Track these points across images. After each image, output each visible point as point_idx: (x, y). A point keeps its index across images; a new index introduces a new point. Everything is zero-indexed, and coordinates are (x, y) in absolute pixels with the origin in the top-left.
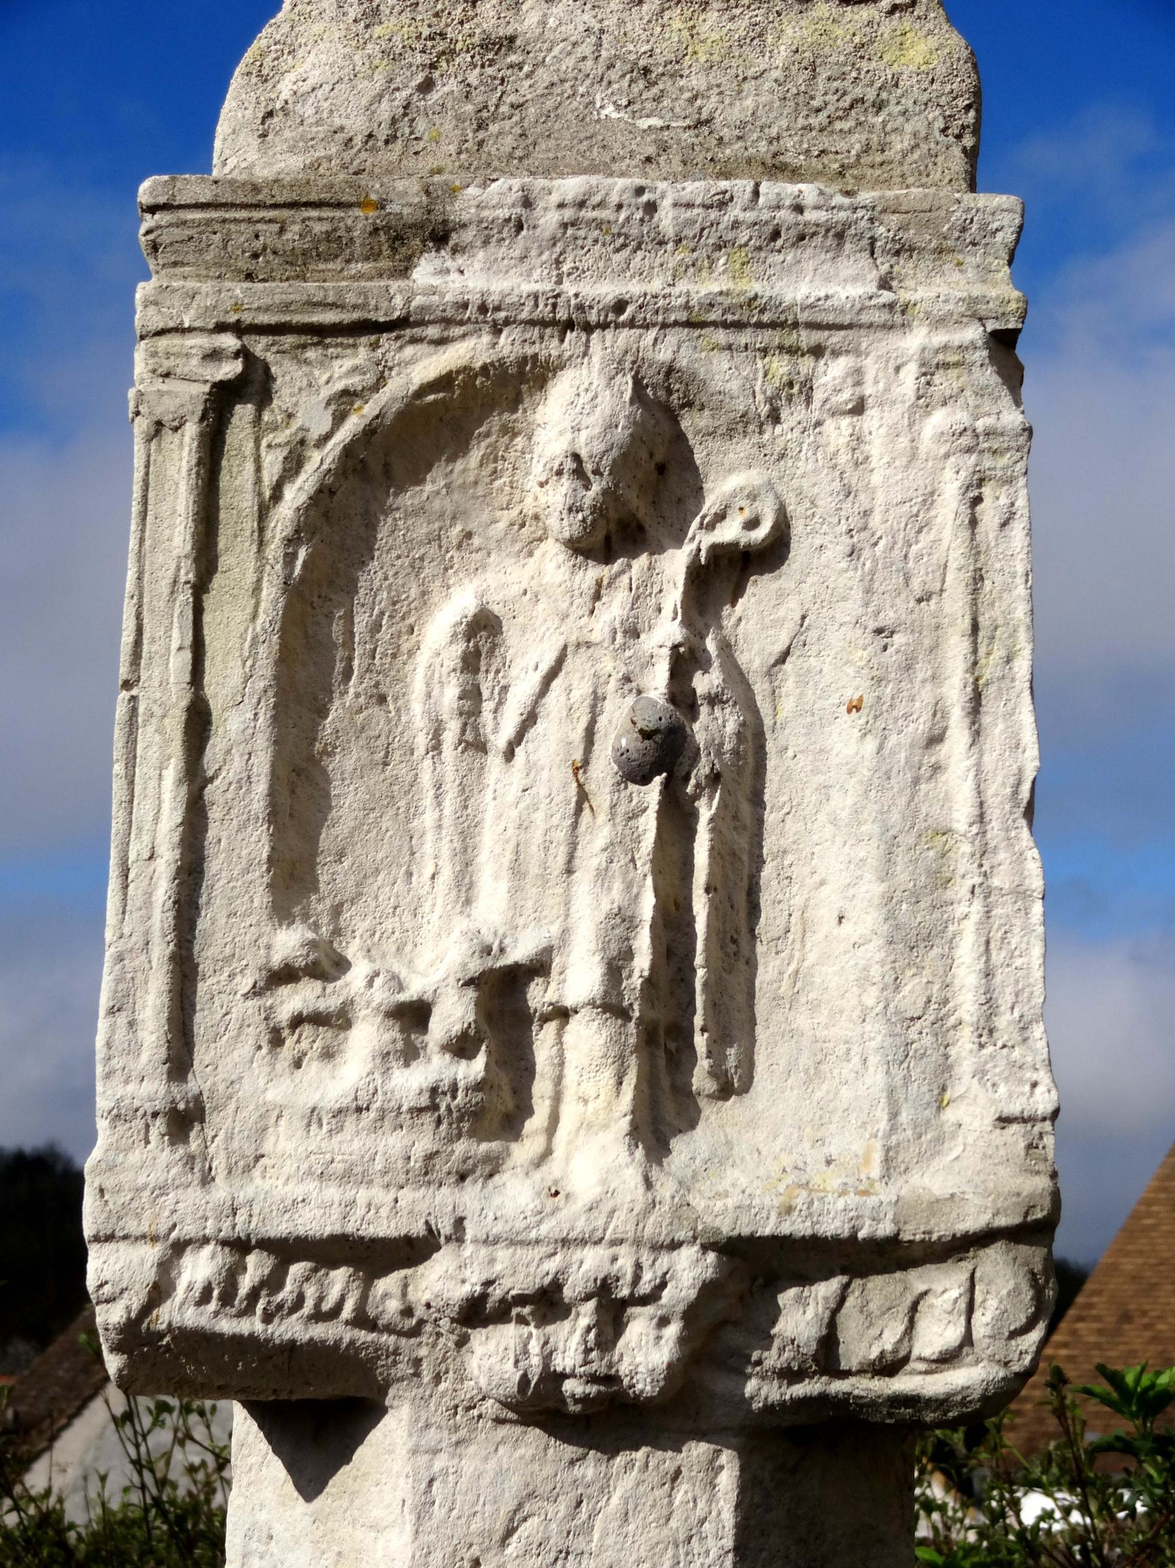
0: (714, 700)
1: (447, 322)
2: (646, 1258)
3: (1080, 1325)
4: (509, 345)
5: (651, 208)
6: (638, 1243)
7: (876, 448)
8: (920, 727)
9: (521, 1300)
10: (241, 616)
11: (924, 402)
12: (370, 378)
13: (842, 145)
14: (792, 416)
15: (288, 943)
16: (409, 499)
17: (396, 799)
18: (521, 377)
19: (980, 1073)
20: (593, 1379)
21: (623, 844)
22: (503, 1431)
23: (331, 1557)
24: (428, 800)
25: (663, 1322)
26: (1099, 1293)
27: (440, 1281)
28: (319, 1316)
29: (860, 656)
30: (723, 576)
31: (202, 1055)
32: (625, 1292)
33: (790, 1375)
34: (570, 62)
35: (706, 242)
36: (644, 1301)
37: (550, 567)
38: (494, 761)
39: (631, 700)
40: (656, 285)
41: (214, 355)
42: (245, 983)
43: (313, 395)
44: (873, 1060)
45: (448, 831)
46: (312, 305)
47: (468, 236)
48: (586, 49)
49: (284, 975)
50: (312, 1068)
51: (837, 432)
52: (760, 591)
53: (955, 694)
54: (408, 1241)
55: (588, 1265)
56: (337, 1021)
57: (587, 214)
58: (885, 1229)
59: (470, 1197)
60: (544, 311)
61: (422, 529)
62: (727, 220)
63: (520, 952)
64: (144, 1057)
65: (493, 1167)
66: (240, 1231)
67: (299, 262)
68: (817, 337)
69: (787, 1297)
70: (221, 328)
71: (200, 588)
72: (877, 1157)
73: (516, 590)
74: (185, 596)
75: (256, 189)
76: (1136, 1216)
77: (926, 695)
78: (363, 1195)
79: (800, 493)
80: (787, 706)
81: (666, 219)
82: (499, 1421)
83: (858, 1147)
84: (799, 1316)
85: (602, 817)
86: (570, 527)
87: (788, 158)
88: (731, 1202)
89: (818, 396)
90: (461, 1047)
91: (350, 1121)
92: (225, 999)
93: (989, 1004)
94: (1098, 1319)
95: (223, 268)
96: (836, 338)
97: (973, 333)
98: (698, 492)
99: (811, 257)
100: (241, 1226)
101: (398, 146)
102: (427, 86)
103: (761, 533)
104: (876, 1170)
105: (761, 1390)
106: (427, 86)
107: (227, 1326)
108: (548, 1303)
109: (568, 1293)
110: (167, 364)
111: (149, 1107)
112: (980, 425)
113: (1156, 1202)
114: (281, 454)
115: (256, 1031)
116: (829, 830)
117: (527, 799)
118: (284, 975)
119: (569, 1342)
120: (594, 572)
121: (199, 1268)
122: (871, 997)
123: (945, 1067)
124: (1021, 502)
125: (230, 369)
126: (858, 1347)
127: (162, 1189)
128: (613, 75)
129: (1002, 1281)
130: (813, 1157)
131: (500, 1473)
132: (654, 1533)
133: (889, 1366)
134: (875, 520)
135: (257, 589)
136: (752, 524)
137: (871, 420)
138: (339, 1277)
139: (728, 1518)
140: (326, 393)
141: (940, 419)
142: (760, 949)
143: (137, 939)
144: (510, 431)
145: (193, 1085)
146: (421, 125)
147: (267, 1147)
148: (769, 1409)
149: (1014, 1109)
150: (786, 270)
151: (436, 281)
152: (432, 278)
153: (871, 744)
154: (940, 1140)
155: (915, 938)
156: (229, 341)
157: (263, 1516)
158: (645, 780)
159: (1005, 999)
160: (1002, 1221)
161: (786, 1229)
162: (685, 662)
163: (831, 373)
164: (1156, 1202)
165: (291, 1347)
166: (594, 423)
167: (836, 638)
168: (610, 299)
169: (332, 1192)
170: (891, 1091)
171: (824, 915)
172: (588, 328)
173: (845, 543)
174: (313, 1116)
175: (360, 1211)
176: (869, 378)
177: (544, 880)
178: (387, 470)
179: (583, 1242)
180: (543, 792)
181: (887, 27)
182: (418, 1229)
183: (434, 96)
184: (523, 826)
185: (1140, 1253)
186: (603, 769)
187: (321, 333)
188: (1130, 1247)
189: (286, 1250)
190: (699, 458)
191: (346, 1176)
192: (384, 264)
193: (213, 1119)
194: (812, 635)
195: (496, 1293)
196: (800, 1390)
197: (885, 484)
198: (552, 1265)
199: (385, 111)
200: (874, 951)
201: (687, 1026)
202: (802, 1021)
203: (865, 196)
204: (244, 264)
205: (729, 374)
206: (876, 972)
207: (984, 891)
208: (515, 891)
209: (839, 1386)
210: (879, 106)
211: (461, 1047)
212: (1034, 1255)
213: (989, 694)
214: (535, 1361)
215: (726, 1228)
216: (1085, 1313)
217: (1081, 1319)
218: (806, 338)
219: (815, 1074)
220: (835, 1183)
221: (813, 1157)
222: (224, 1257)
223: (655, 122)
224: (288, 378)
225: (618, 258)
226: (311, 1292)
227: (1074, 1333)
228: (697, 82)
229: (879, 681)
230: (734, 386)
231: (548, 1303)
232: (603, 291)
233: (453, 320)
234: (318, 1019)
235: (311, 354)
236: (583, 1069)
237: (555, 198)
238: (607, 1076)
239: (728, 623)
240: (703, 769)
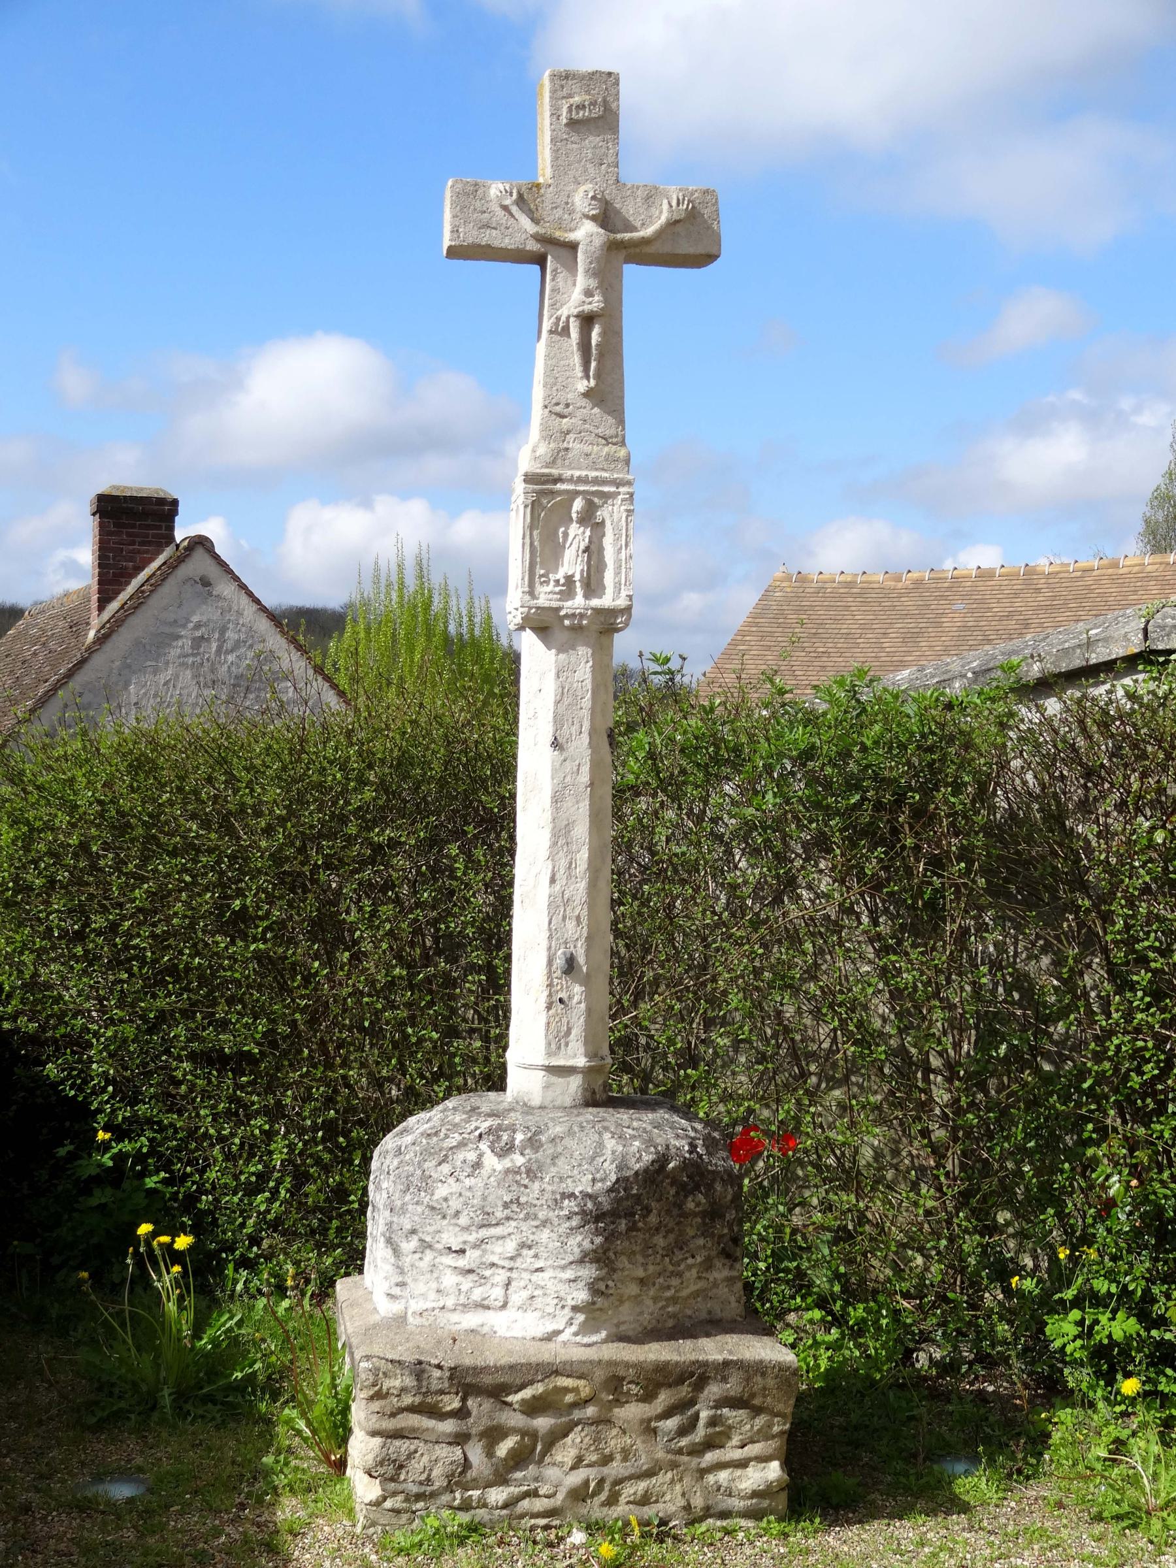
113: (750, 633)
164: (750, 633)
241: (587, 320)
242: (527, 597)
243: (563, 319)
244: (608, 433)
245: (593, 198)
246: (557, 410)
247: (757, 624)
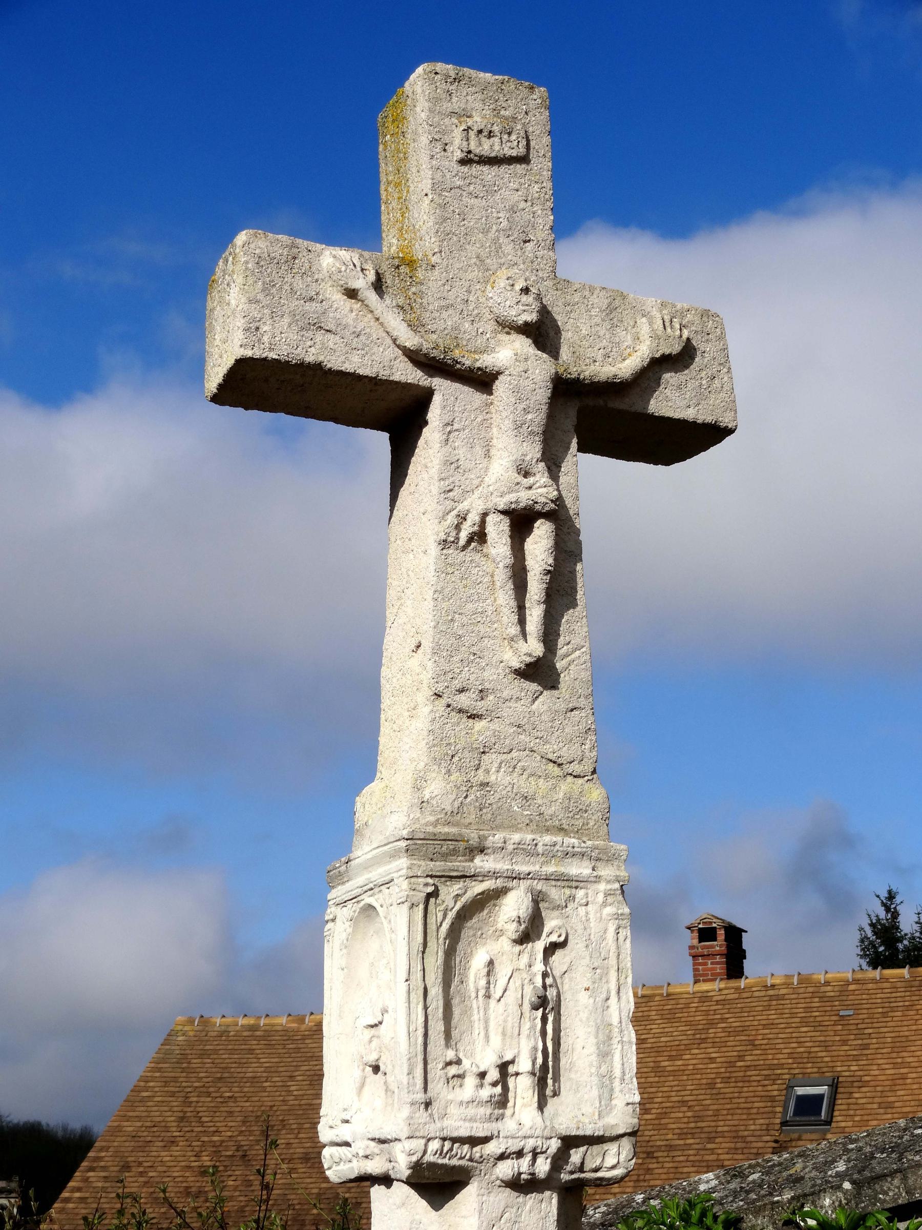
0: (551, 986)
1: (485, 876)
2: (544, 1141)
3: (91, 1174)
4: (499, 883)
5: (536, 845)
6: (542, 1137)
7: (591, 916)
8: (604, 996)
9: (514, 1153)
10: (433, 960)
11: (604, 904)
12: (463, 891)
13: (577, 823)
14: (571, 906)
15: (450, 1055)
16: (469, 924)
17: (467, 1011)
18: (501, 891)
19: (621, 1091)
20: (530, 1174)
21: (533, 1027)
22: (500, 1189)
23: (446, 1227)
24: (476, 1012)
25: (547, 1158)
26: (106, 1149)
27: (493, 1148)
28: (461, 1158)
29: (589, 975)
30: (551, 949)
31: (430, 1086)
32: (539, 1151)
33: (572, 1173)
34: (505, 792)
35: (550, 855)
36: (542, 1153)
37: (505, 945)
38: (492, 1002)
39: (532, 986)
40: (537, 868)
41: (426, 885)
42: (440, 1066)
43: (453, 896)
44: (594, 1087)
45: (482, 1022)
46: (451, 870)
47: (489, 851)
48: (509, 789)
49: (449, 1063)
50: (457, 1090)
51: (582, 910)
52: (559, 954)
53: (613, 986)
54: (486, 1137)
55: (530, 1144)
56: (461, 1076)
57: (521, 846)
58: (601, 1133)
59: (499, 1125)
60: (509, 874)
61: (471, 933)
62: (555, 850)
63: (508, 1058)
64: (418, 1087)
65: (502, 1117)
66: (445, 1135)
67: (445, 856)
68: (577, 884)
69: (572, 1151)
70: (427, 876)
71: (423, 952)
72: (597, 1114)
73: (497, 952)
74: (420, 955)
75: (435, 835)
76: (136, 1090)
77: (605, 988)
78: (475, 1125)
79: (572, 927)
80: (566, 987)
81: (540, 849)
82: (500, 1186)
83: (591, 1110)
84: (576, 1156)
85: (527, 1020)
86: (515, 936)
87: (563, 826)
88: (565, 1126)
89: (577, 900)
90: (494, 1084)
91: (470, 1104)
92: (436, 1069)
93: (624, 1073)
94: (104, 1168)
95: (425, 857)
96: (582, 884)
97: (617, 886)
98: (543, 925)
99: (575, 861)
100: (445, 1134)
101: (459, 815)
102: (466, 797)
103: (562, 939)
104: (596, 1117)
105: (565, 1177)
106: (466, 797)
107: (440, 1161)
108: (520, 1154)
109: (525, 1151)
110: (414, 887)
111: (421, 1101)
112: (620, 912)
113: (153, 1079)
114: (442, 913)
115: (443, 1080)
116: (579, 1023)
117: (506, 1014)
118: (449, 1063)
119: (524, 1164)
120: (518, 948)
121: (434, 1145)
122: (593, 1070)
123: (612, 1090)
124: (629, 934)
125: (430, 889)
126: (589, 1165)
127: (425, 1124)
128: (517, 797)
129: (626, 1145)
130: (579, 1114)
131: (500, 1200)
132: (537, 1216)
133: (596, 1170)
134: (592, 936)
135: (437, 952)
136: (560, 936)
137: (590, 907)
138: (466, 1147)
139: (555, 1212)
140: (453, 895)
141: (609, 910)
142: (561, 1055)
143: (414, 1054)
144: (495, 905)
145: (429, 1094)
146: (465, 809)
147: (448, 1111)
148: (566, 1182)
149: (630, 1101)
150: (569, 864)
151: (481, 864)
152: (481, 863)
153: (592, 1000)
154: (611, 1109)
155: (604, 1055)
156: (430, 880)
157: (417, 1217)
158: (537, 1009)
159: (627, 1071)
160: (628, 1131)
161: (578, 1133)
162: (545, 975)
163: (580, 893)
164: (153, 1079)
165: (454, 1167)
166: (524, 907)
167: (581, 969)
168: (527, 872)
169: (467, 1124)
170: (600, 1096)
171: (578, 1047)
172: (520, 879)
173: (584, 944)
174: (461, 1103)
175: (474, 1129)
176: (590, 895)
177: (512, 1037)
178: (465, 916)
179: (529, 1137)
180: (511, 1012)
181: (587, 786)
182: (489, 1134)
183: (468, 799)
184: (505, 1021)
185: (139, 1118)
186: (527, 1007)
187: (451, 878)
188: (131, 1114)
189: (454, 1140)
190: (543, 914)
191: (471, 1120)
192: (467, 858)
193: (433, 1104)
194: (574, 967)
195: (508, 1151)
196: (574, 1176)
197: (595, 927)
198: (522, 1143)
199: (456, 804)
200: (594, 1058)
201: (546, 1079)
202: (573, 1076)
203: (589, 843)
204: (431, 856)
205: (556, 894)
206: (595, 1063)
207: (621, 1042)
208: (504, 1039)
209: (582, 1175)
210: (586, 811)
211: (494, 1084)
212: (633, 1139)
213: (621, 988)
214: (516, 1169)
215: (564, 1134)
216: (95, 1165)
217: (92, 1169)
218: (574, 884)
219: (577, 1091)
220: (587, 1121)
221: (579, 1114)
222: (441, 1142)
223: (528, 812)
224: (443, 890)
225: (527, 859)
226: (459, 1151)
227: (86, 1180)
228: (540, 802)
229: (594, 982)
230: (556, 897)
231: (520, 1154)
232: (524, 869)
233: (486, 876)
234: (459, 1076)
235: (448, 883)
236: (523, 1088)
237: (512, 841)
238: (531, 1091)
239: (551, 962)
240: (550, 1006)
241: (521, 521)
242: (422, 1115)
243: (473, 518)
244: (566, 753)
245: (526, 291)
246: (461, 705)
247: (160, 1070)
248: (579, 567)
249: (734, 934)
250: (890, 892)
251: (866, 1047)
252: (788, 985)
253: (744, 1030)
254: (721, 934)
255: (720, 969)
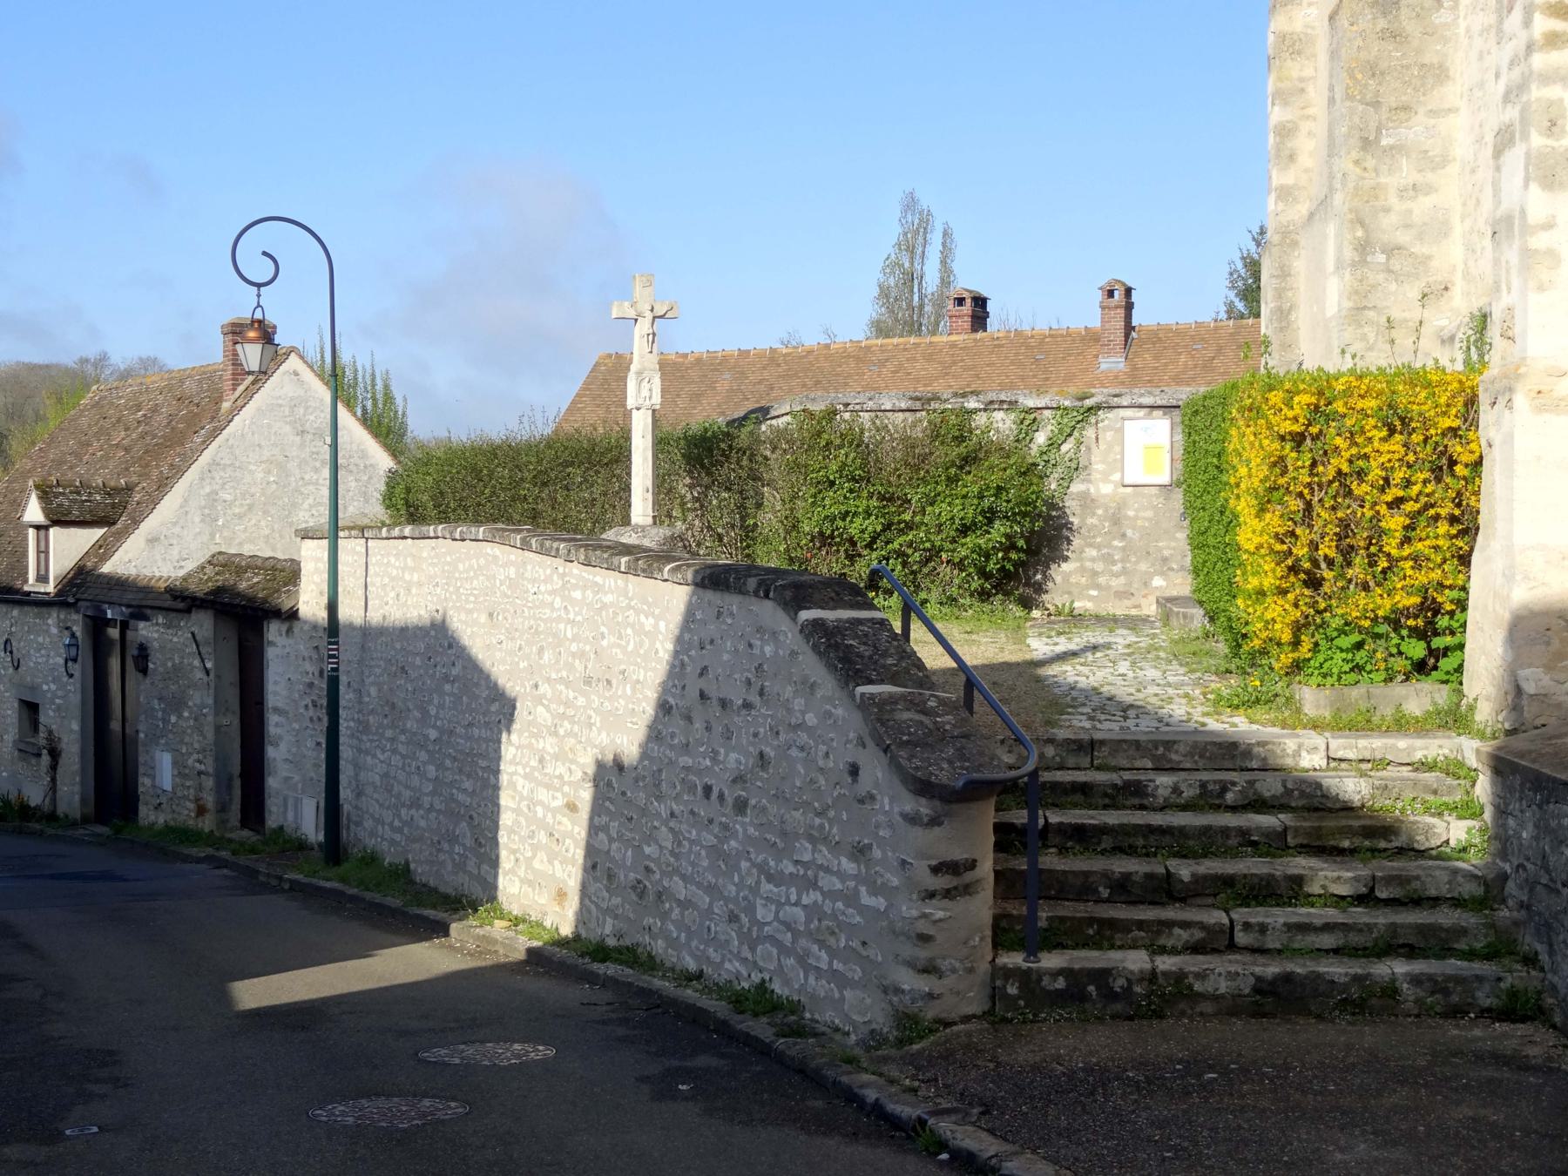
248: (628, 743)
249: (980, 302)
250: (1262, 228)
251: (1047, 379)
252: (1007, 338)
253: (975, 366)
254: (968, 301)
255: (967, 325)
